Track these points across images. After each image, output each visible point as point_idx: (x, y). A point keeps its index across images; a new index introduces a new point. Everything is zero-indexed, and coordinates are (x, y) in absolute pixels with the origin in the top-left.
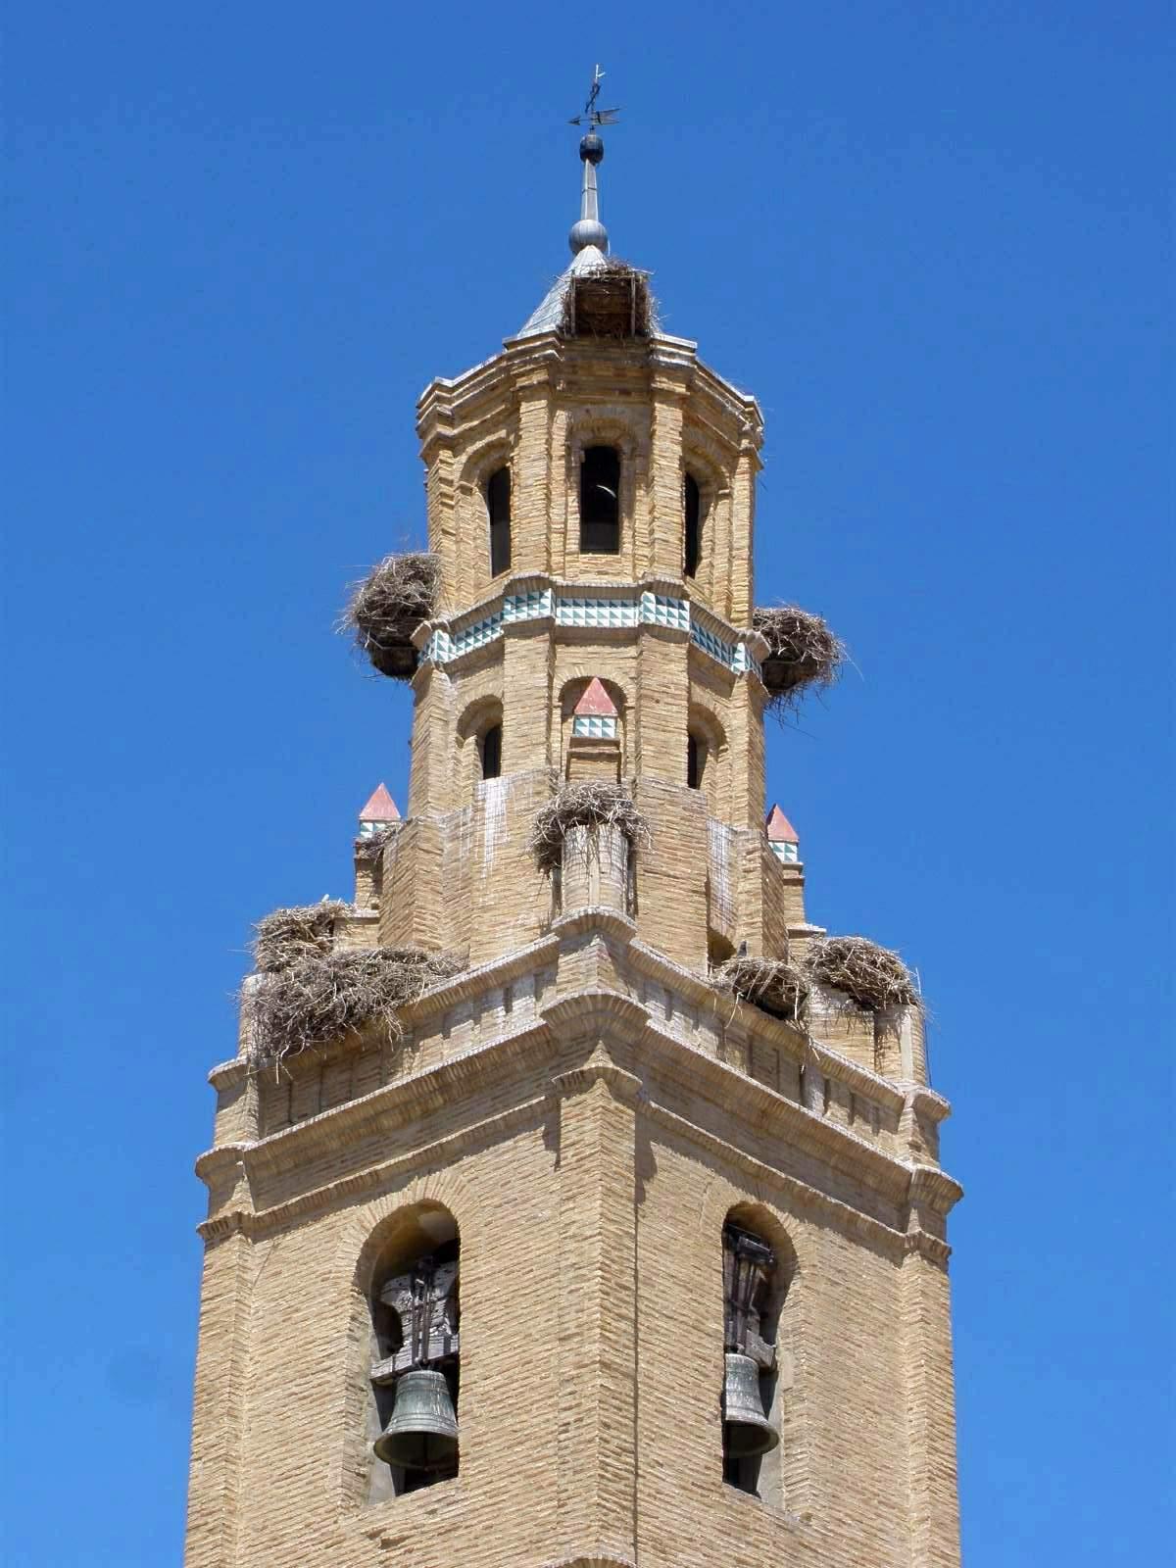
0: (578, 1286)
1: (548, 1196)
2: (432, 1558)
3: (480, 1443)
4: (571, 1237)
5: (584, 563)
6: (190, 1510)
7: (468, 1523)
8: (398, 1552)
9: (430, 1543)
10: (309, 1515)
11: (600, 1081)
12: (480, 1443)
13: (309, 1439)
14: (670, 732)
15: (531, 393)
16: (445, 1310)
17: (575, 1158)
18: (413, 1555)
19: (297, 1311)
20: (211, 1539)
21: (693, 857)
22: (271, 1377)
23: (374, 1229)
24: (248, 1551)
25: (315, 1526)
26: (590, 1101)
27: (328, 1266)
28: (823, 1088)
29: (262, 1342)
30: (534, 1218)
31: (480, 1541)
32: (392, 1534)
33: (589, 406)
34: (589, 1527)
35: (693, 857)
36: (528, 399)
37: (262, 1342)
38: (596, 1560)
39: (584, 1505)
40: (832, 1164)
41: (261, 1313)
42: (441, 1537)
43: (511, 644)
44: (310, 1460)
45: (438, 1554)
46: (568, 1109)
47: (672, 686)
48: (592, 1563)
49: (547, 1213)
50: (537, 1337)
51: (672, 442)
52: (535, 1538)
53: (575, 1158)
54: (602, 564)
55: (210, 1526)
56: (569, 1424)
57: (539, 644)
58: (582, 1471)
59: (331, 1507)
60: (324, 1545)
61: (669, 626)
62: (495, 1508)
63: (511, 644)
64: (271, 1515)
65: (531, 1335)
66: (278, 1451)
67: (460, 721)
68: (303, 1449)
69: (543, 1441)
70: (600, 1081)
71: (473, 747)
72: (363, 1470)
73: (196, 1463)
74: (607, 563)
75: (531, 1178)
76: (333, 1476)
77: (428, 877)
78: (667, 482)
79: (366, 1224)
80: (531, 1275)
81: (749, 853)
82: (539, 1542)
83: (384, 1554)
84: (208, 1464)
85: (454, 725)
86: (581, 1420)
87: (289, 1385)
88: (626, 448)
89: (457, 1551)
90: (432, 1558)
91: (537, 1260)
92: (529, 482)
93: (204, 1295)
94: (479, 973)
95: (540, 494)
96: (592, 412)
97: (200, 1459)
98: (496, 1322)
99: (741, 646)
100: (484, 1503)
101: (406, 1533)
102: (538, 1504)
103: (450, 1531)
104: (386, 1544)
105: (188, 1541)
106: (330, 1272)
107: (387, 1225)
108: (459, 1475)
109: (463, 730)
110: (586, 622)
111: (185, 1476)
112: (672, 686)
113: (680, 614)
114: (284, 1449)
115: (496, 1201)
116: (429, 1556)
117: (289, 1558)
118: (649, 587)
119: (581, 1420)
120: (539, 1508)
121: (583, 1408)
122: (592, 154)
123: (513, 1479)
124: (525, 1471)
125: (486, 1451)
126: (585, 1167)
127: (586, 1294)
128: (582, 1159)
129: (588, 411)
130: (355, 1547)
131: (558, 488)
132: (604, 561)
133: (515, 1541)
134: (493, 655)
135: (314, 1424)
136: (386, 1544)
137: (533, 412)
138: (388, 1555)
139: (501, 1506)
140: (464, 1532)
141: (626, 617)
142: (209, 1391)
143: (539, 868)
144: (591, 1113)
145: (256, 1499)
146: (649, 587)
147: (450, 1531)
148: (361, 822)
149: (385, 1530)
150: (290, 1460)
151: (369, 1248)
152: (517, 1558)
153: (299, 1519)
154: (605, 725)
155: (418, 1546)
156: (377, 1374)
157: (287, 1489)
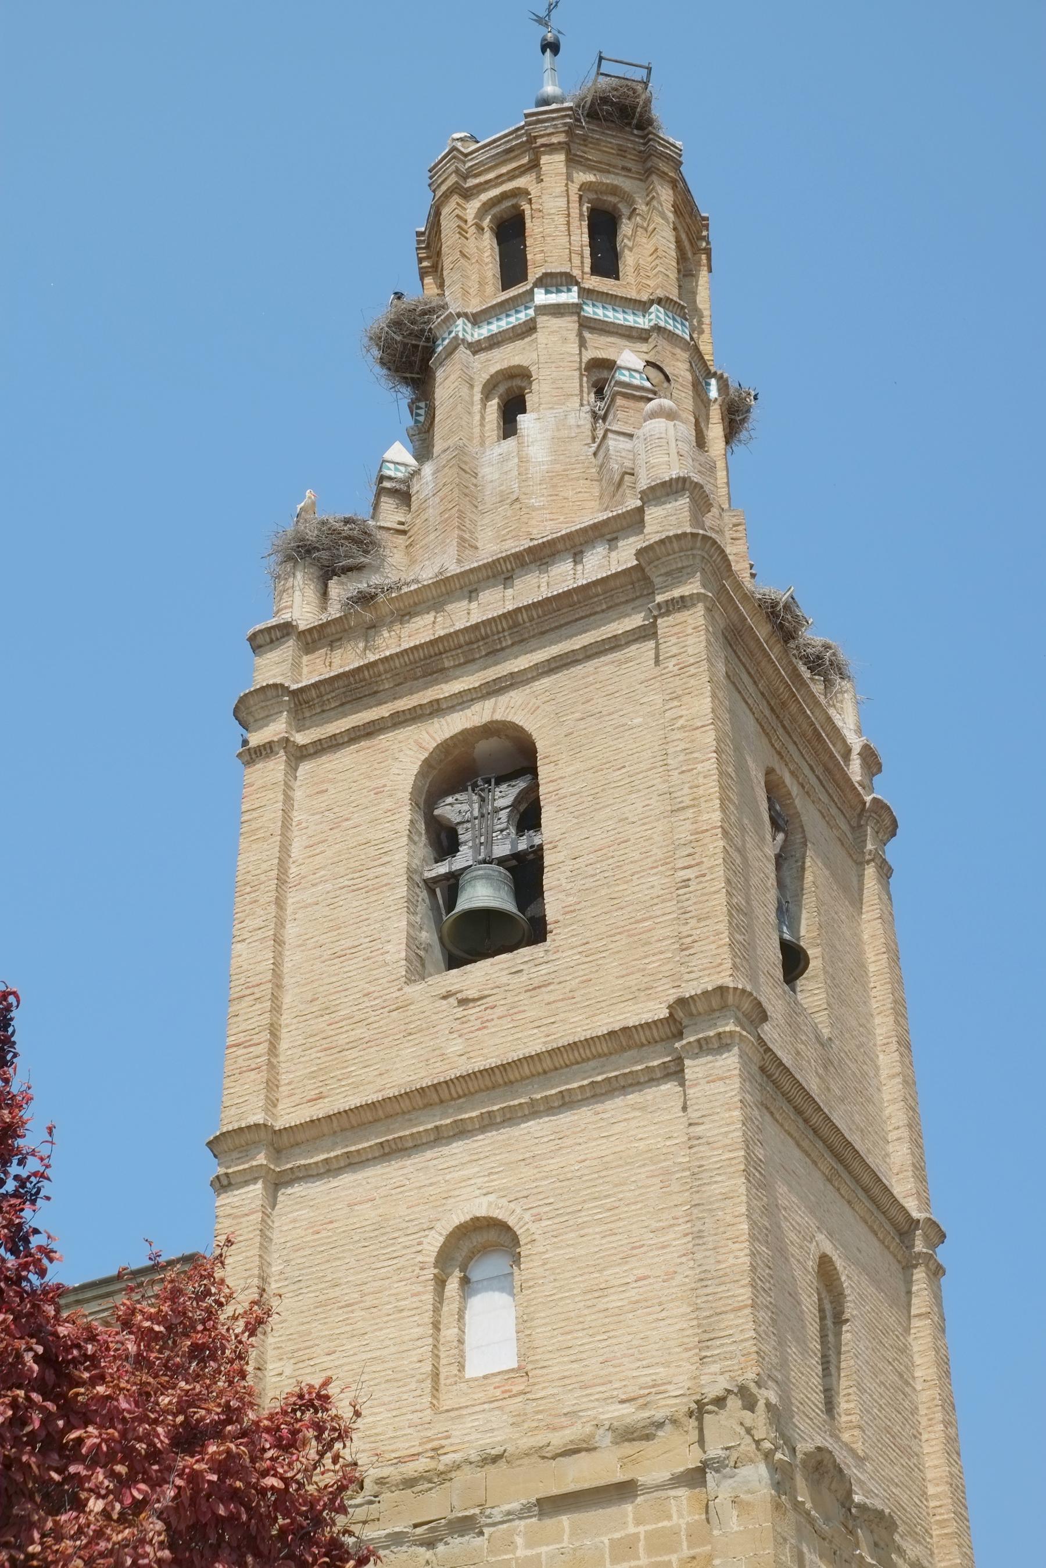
0: (690, 767)
1: (638, 707)
2: (520, 1012)
3: (574, 911)
4: (679, 729)
6: (232, 984)
7: (562, 979)
8: (478, 1009)
9: (516, 999)
10: (367, 985)
11: (700, 605)
12: (574, 911)
13: (366, 923)
15: (552, 148)
16: (509, 817)
17: (677, 667)
18: (495, 1010)
19: (347, 820)
20: (258, 1006)
22: (317, 875)
24: (295, 1021)
25: (376, 995)
26: (691, 622)
27: (383, 781)
29: (307, 847)
30: (623, 725)
31: (575, 994)
32: (472, 993)
34: (721, 964)
36: (550, 153)
37: (307, 847)
38: (735, 989)
39: (713, 946)
40: (383, 1117)
41: (304, 825)
42: (529, 994)
43: (542, 321)
44: (368, 940)
45: (526, 1008)
46: (667, 630)
48: (731, 991)
49: (638, 721)
50: (634, 820)
52: (643, 986)
55: (257, 996)
56: (689, 880)
57: (569, 324)
58: (708, 918)
59: (393, 977)
60: (387, 1009)
62: (593, 964)
63: (542, 321)
64: (321, 989)
65: (627, 819)
66: (329, 935)
67: (485, 386)
68: (359, 931)
69: (648, 905)
70: (700, 605)
71: (496, 407)
72: (422, 953)
73: (239, 945)
75: (617, 695)
76: (396, 950)
77: (467, 491)
78: (664, 234)
79: (424, 744)
80: (624, 770)
81: (735, 525)
82: (647, 989)
83: (459, 1012)
84: (254, 944)
85: (478, 389)
86: (704, 875)
87: (341, 880)
88: (625, 211)
89: (549, 1004)
90: (520, 1012)
91: (630, 758)
92: (553, 211)
93: (244, 808)
94: (549, 538)
95: (563, 220)
97: (244, 940)
98: (585, 811)
99: (713, 382)
100: (580, 961)
101: (486, 993)
102: (645, 957)
103: (539, 987)
104: (463, 1002)
105: (230, 1009)
106: (385, 786)
107: (445, 748)
108: (548, 939)
109: (487, 394)
111: (228, 956)
114: (335, 933)
115: (577, 715)
116: (516, 1010)
117: (344, 1023)
118: (659, 301)
119: (704, 875)
120: (647, 961)
121: (704, 866)
122: (552, 47)
123: (614, 939)
124: (628, 931)
125: (579, 918)
126: (690, 673)
127: (699, 773)
130: (424, 1009)
131: (575, 222)
133: (620, 990)
134: (529, 328)
135: (371, 910)
136: (463, 1002)
137: (554, 163)
138: (465, 1013)
139: (601, 962)
140: (557, 987)
141: (642, 322)
142: (252, 884)
145: (303, 976)
146: (659, 301)
147: (539, 987)
148: (384, 461)
149: (461, 991)
150: (343, 942)
151: (427, 765)
152: (622, 1005)
153: (356, 990)
155: (502, 1002)
156: (428, 875)
157: (340, 965)
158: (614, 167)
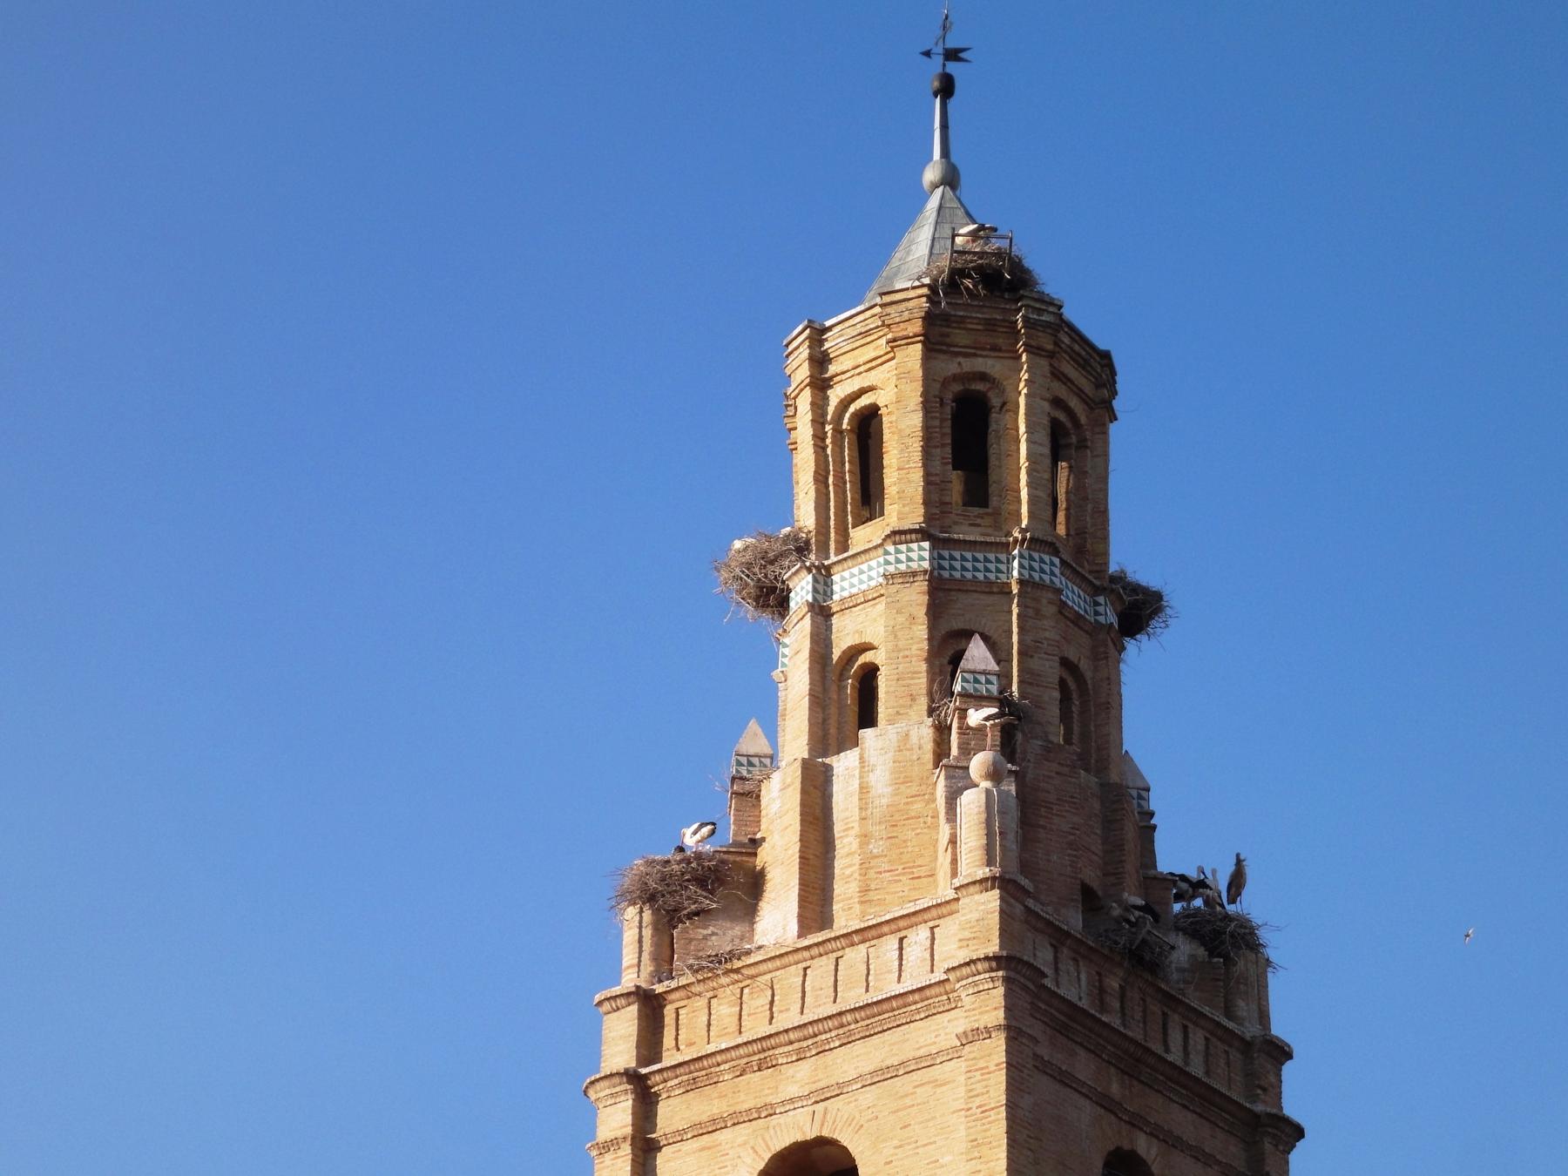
5: (957, 515)
14: (1043, 686)
17: (980, 1110)
21: (1067, 811)
23: (966, 372)
28: (1053, 966)
33: (960, 359)
35: (1067, 811)
47: (1045, 642)
51: (1042, 399)
53: (980, 1110)
54: (975, 516)
61: (1042, 582)
74: (979, 516)
96: (964, 365)
110: (962, 575)
112: (1045, 642)
113: (1051, 570)
115: (896, 1142)
128: (986, 1111)
129: (959, 363)
132: (976, 514)
143: (763, 869)
144: (995, 1068)
154: (988, 682)
158: (983, 349)
